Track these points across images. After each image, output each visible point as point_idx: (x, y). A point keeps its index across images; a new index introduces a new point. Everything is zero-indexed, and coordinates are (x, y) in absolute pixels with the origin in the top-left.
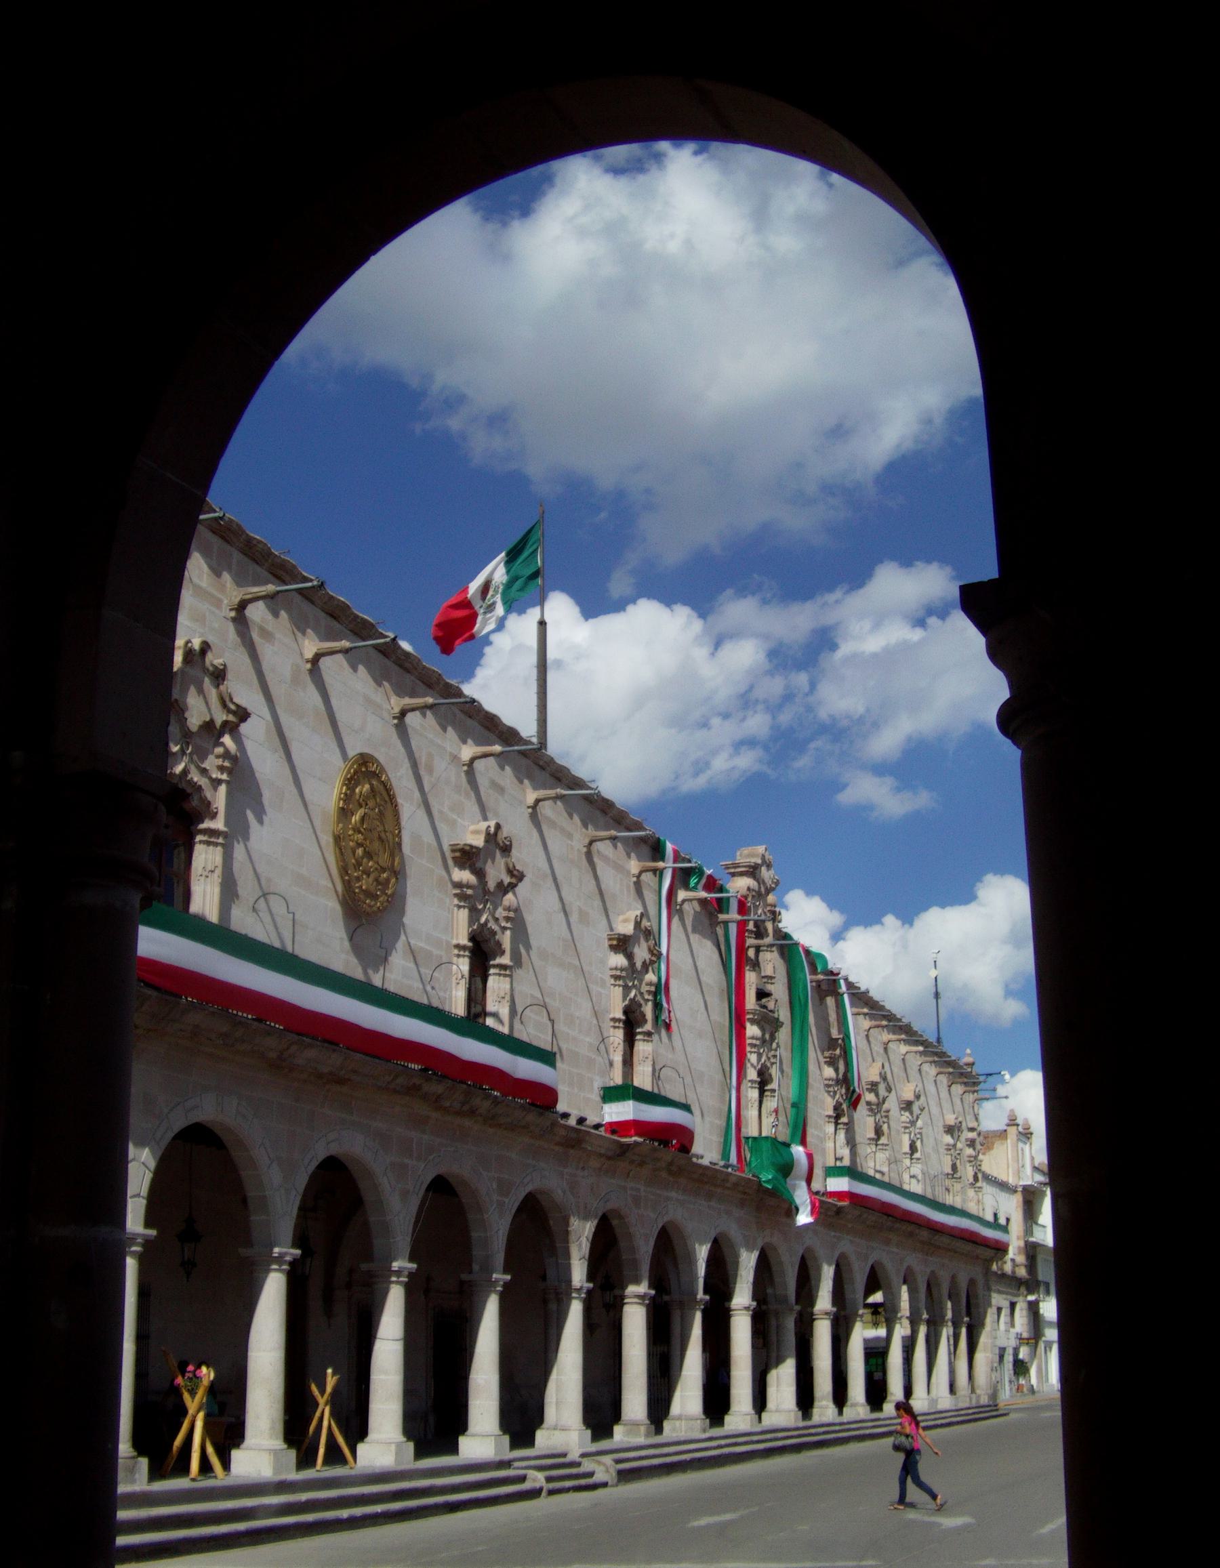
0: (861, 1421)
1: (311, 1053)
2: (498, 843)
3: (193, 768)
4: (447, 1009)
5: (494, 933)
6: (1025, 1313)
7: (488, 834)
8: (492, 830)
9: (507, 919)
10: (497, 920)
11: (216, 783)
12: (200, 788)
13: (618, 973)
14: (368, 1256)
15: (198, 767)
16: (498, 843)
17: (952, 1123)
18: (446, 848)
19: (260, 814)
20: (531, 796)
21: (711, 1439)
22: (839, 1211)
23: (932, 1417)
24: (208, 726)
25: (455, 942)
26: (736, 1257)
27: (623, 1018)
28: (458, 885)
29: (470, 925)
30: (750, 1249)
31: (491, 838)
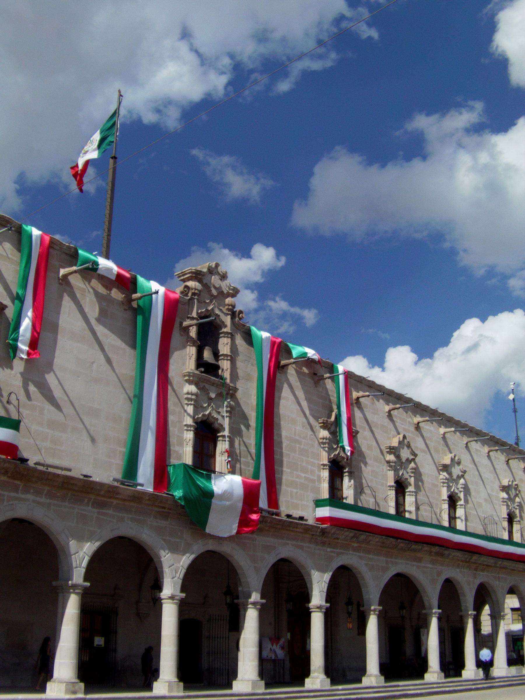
0: (514, 677)
1: (500, 563)
2: (456, 462)
3: (405, 473)
4: (496, 536)
5: (457, 494)
6: (70, 568)
7: (452, 459)
8: (453, 457)
9: (412, 473)
10: (458, 489)
11: (461, 491)
12: (217, 419)
13: (190, 396)
14: (424, 607)
15: (216, 411)
16: (456, 462)
17: (507, 484)
18: (383, 448)
19: (366, 464)
20: (387, 408)
21: (444, 683)
22: (323, 532)
23: (471, 683)
24: (407, 459)
25: (322, 463)
26: (309, 575)
27: (507, 517)
28: (388, 462)
29: (448, 492)
30: (322, 570)
31: (452, 460)
